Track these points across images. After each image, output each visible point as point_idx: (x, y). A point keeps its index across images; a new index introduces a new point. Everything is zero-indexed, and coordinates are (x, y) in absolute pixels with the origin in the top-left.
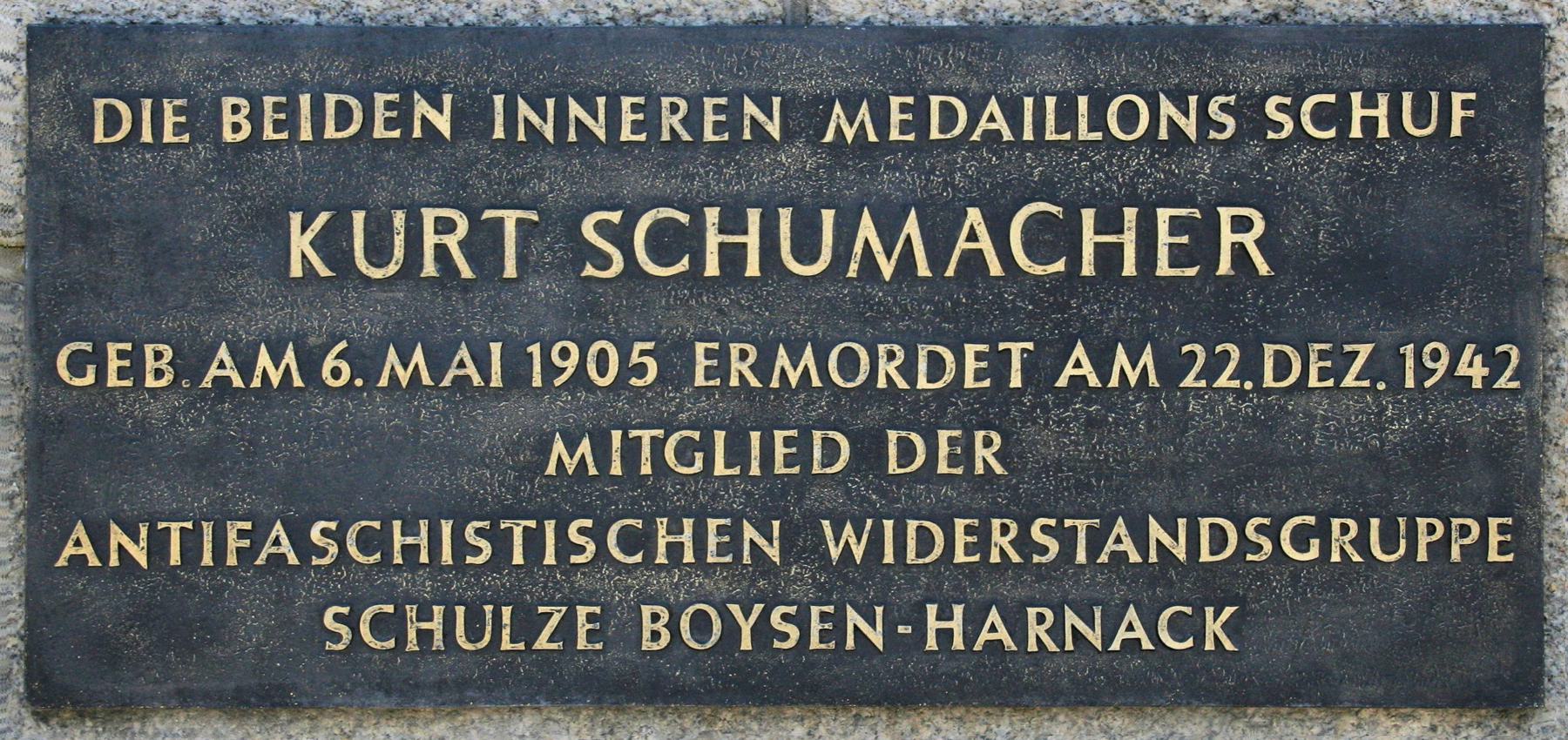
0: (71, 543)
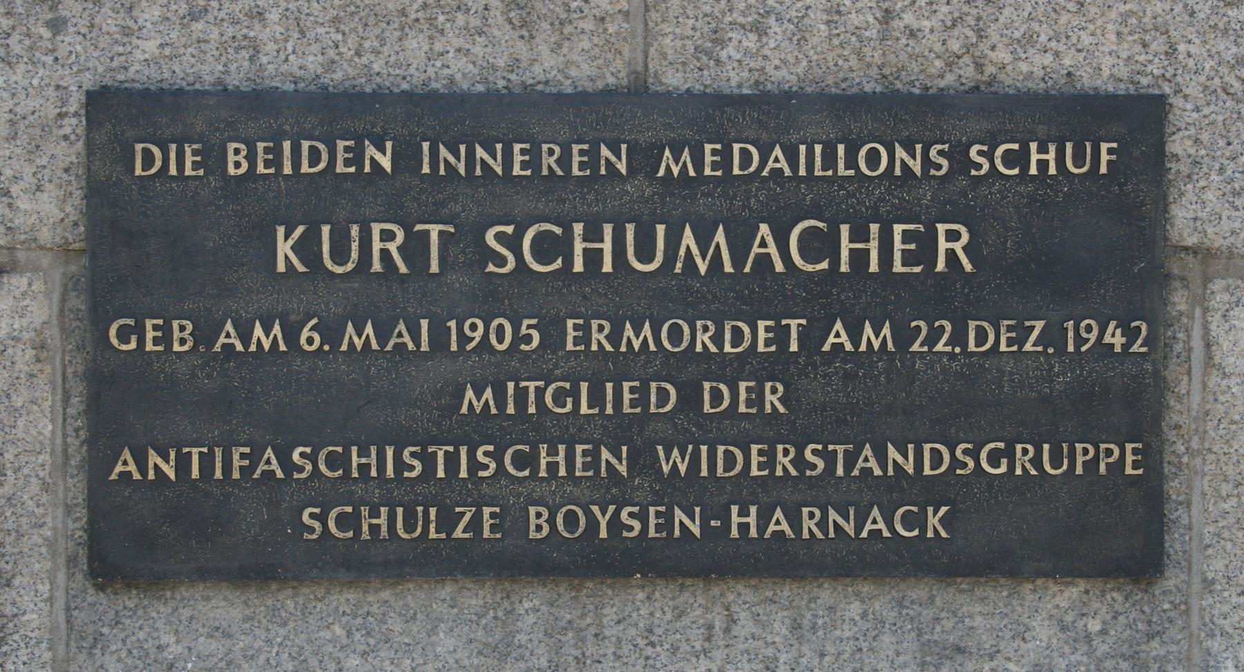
0: (120, 463)
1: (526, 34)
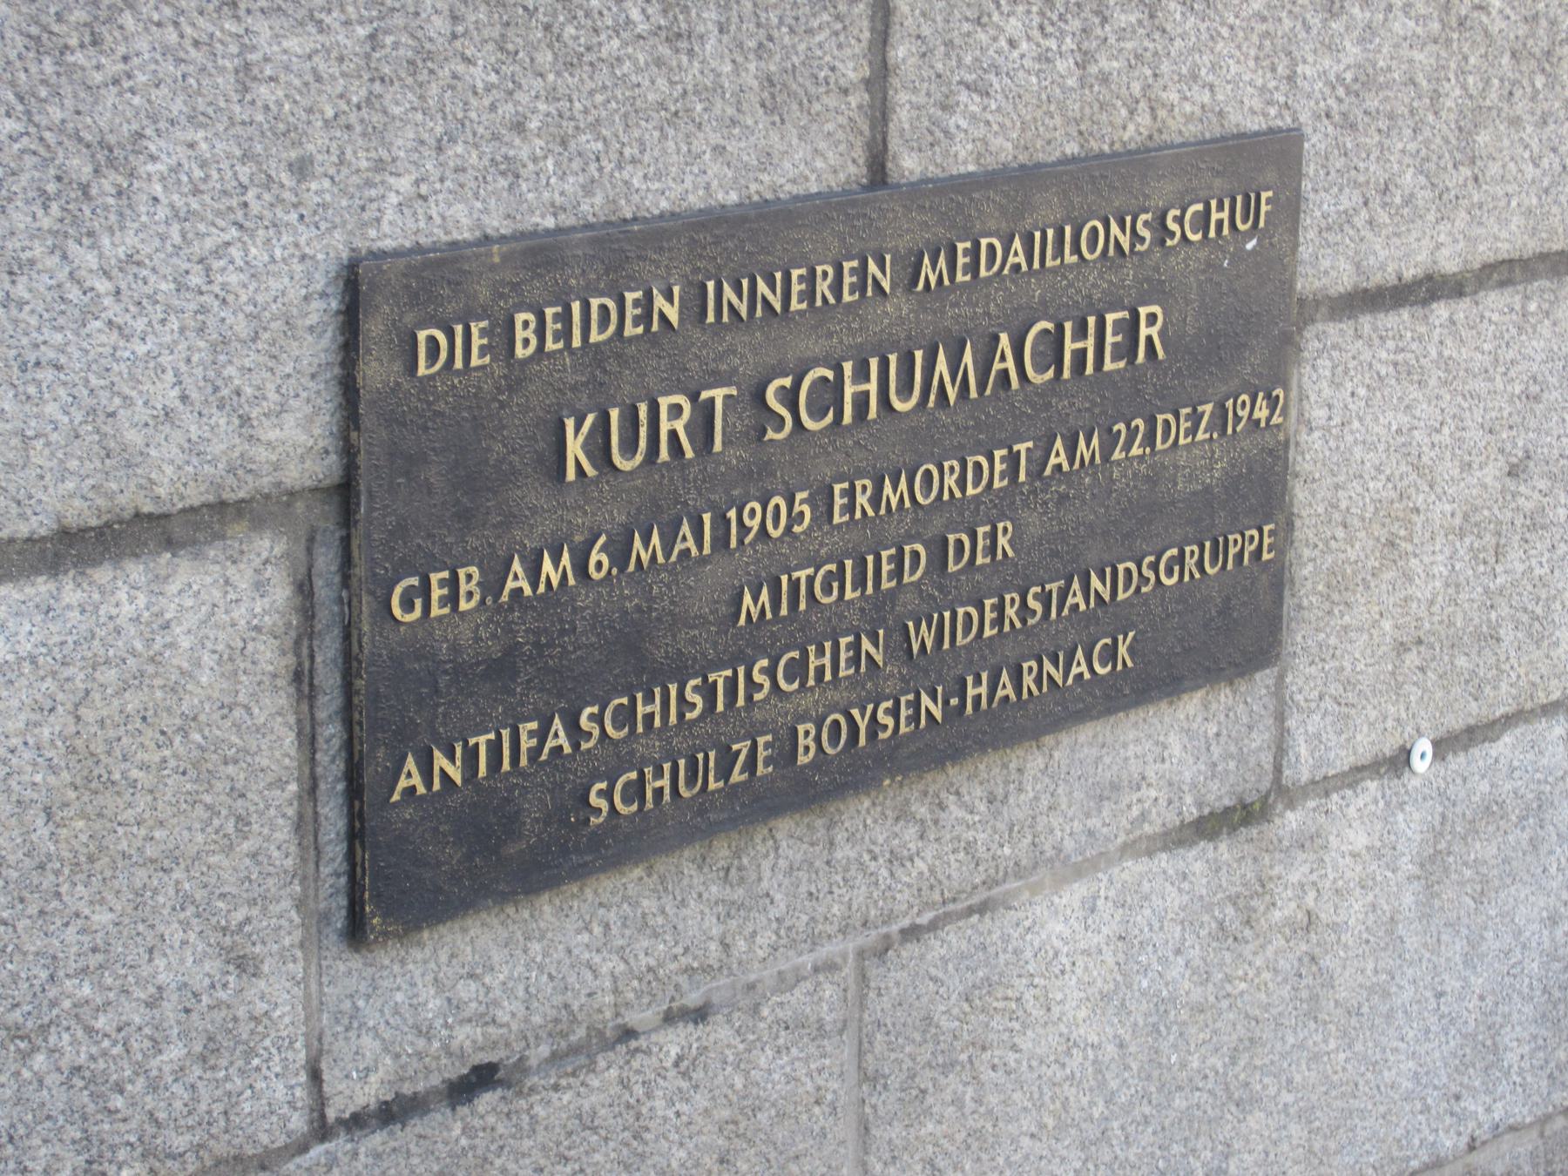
0: (403, 777)
1: (777, 119)
